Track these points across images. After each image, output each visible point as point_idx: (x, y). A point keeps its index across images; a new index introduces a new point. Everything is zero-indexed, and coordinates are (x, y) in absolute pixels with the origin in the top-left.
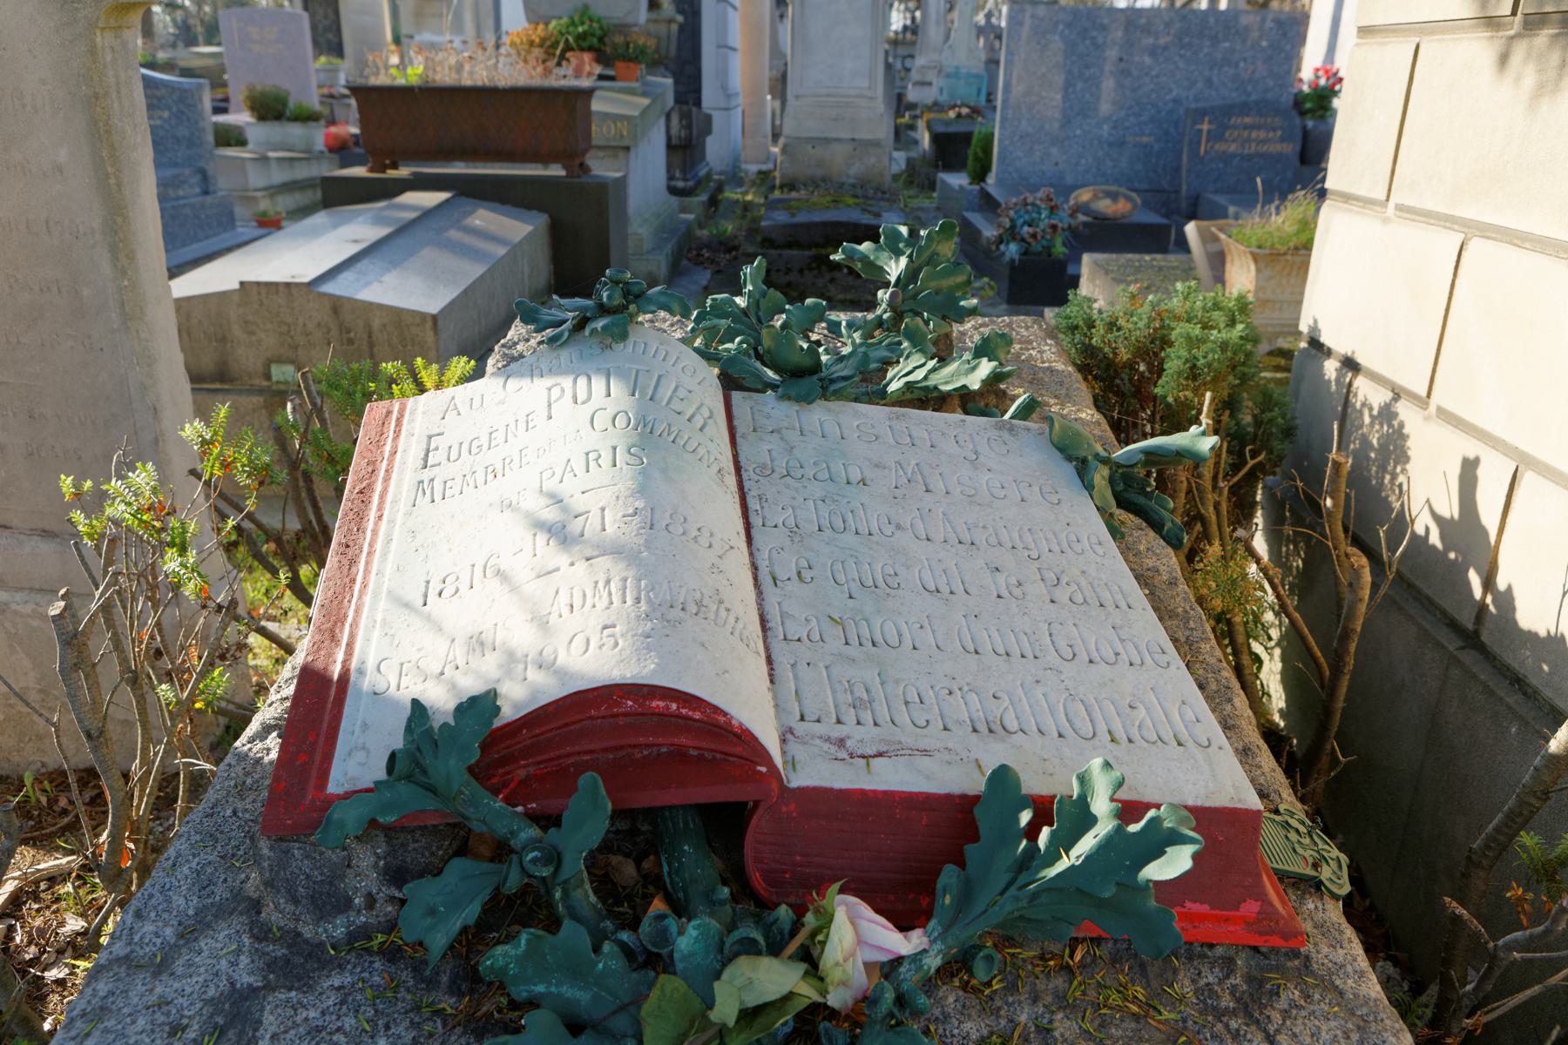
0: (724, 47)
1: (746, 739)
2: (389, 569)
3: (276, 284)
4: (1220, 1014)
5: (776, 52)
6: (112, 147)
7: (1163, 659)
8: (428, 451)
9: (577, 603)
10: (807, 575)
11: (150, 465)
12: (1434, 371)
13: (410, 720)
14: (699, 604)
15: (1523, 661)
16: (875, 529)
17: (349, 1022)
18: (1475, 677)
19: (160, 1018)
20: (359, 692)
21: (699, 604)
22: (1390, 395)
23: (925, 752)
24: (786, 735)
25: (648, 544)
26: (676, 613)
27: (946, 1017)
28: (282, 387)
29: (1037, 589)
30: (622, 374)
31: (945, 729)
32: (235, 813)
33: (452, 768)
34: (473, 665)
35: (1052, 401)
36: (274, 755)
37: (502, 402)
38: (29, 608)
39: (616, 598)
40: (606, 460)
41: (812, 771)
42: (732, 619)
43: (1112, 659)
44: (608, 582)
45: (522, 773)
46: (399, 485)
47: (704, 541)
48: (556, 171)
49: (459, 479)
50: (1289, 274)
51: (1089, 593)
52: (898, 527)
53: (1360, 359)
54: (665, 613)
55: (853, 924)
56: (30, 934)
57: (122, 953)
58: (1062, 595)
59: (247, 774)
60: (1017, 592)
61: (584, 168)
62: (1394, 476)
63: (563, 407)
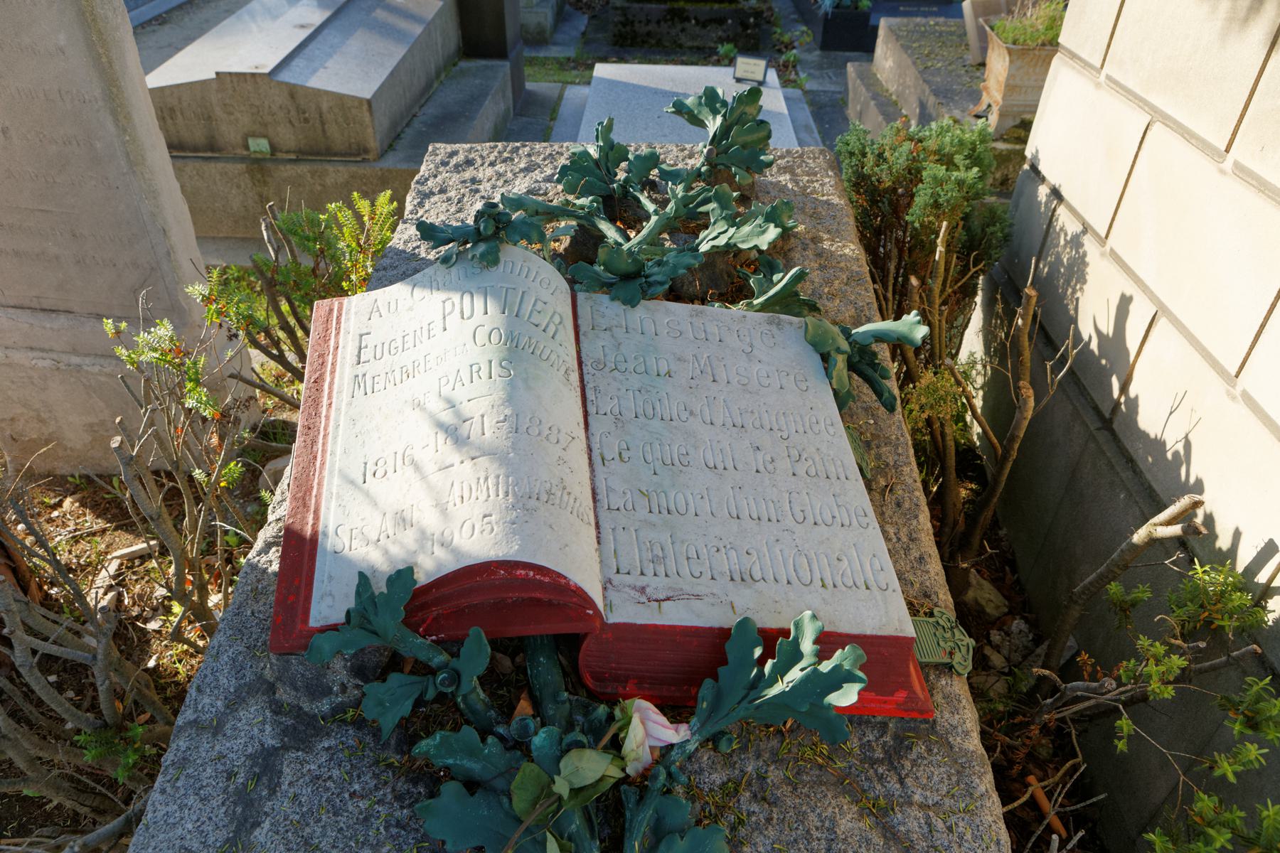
1: (581, 596)
2: (339, 451)
3: (244, 74)
4: (873, 762)
6: (100, 33)
7: (864, 521)
8: (360, 349)
9: (466, 496)
10: (625, 455)
11: (166, 321)
12: (1113, 219)
13: (358, 586)
14: (549, 493)
15: (1136, 450)
16: (675, 416)
17: (336, 773)
18: (1103, 453)
19: (220, 768)
20: (325, 550)
21: (549, 493)
22: (1080, 228)
23: (698, 597)
24: (607, 585)
25: (514, 447)
26: (533, 503)
27: (702, 770)
28: (259, 156)
29: (784, 465)
30: (496, 296)
31: (713, 578)
32: (253, 613)
33: (390, 624)
34: (399, 536)
35: (826, 236)
36: (275, 567)
37: (411, 309)
38: (97, 369)
39: (492, 492)
40: (484, 373)
41: (625, 612)
42: (572, 501)
43: (829, 521)
44: (486, 479)
45: (435, 614)
46: (342, 378)
47: (553, 439)
49: (383, 376)
50: (1036, 65)
51: (820, 467)
52: (692, 413)
53: (1064, 193)
54: (526, 503)
55: (643, 723)
56: (133, 598)
57: (192, 718)
58: (801, 470)
59: (259, 581)
60: (770, 467)
62: (1074, 292)
63: (453, 320)
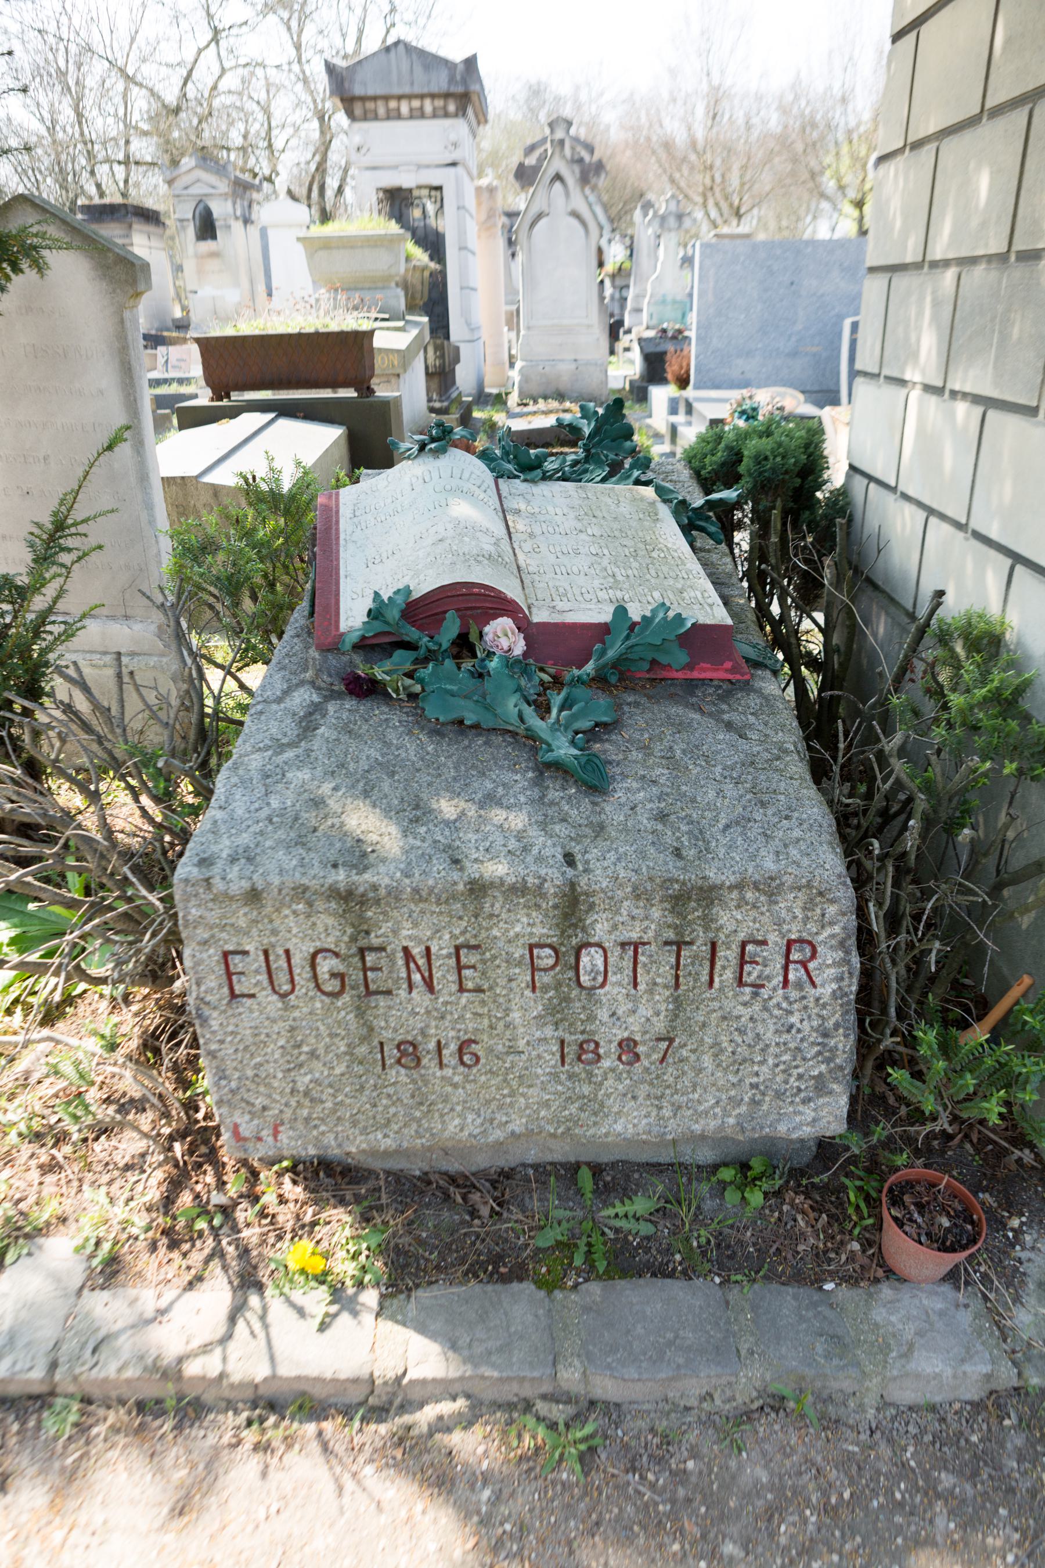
0: (466, 288)
5: (511, 291)
48: (350, 393)
61: (370, 391)
